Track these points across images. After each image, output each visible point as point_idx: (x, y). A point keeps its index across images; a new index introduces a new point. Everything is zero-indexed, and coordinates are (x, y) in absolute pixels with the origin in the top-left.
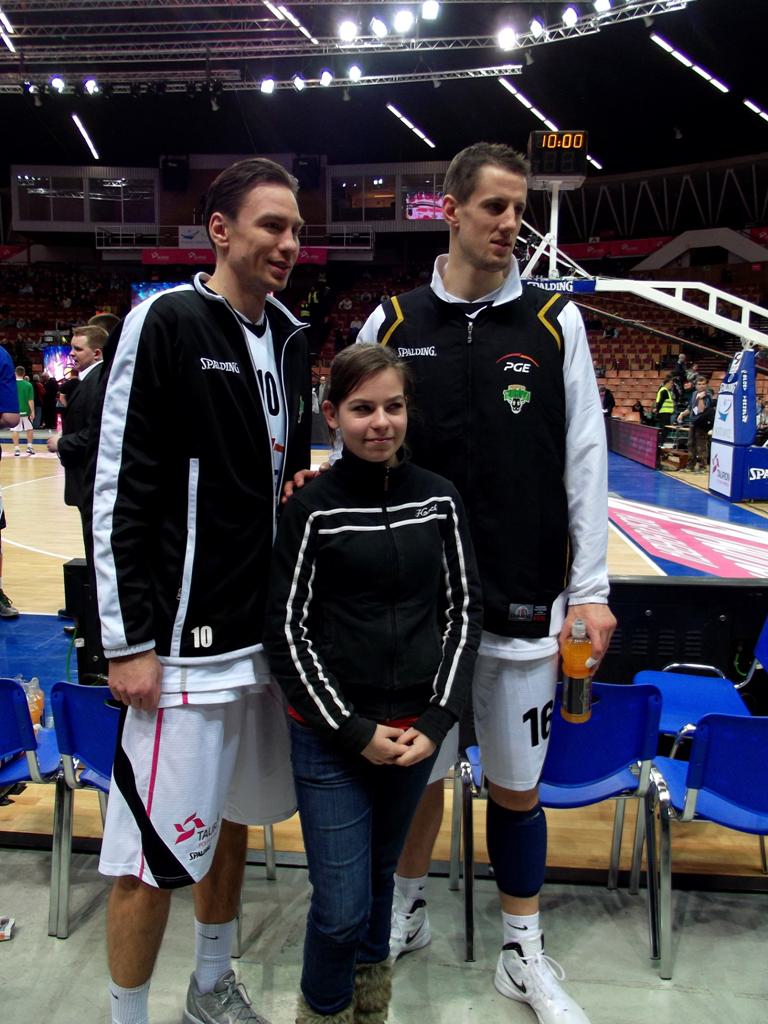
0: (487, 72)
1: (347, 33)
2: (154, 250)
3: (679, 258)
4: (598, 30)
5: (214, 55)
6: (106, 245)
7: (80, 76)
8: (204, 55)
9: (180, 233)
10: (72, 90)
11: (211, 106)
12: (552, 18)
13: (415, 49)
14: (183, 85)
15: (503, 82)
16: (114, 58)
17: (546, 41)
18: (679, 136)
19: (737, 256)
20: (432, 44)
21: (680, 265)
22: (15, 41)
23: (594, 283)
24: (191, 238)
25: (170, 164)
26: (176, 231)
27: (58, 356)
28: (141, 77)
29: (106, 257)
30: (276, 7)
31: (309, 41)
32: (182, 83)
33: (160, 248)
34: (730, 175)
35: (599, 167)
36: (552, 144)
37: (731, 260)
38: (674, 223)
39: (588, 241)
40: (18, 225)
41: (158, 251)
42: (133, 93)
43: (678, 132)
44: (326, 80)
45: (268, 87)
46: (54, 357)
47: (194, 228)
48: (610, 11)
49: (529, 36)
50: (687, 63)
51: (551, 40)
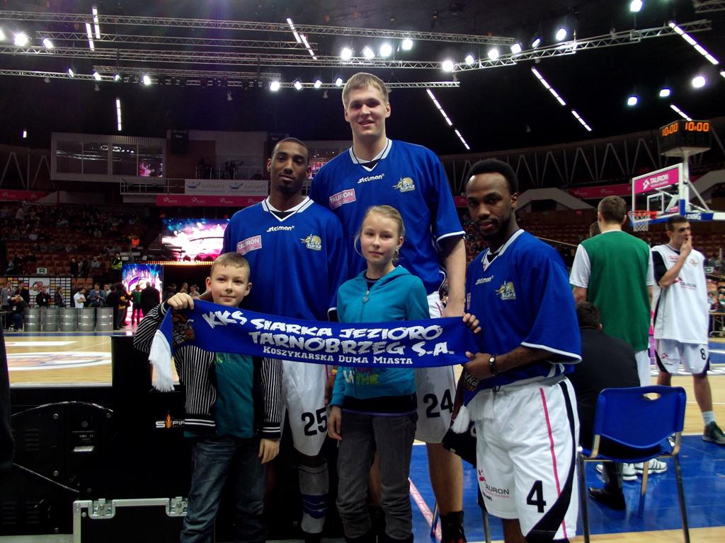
0: (419, 85)
1: (346, 55)
2: (166, 196)
3: (525, 206)
4: (515, 64)
5: (262, 63)
6: (126, 192)
7: (266, 75)
8: (255, 63)
9: (186, 184)
10: (157, 82)
11: (227, 97)
12: (480, 52)
13: (402, 67)
14: (199, 81)
15: (429, 92)
16: (234, 62)
17: (480, 68)
18: (529, 130)
19: (563, 205)
20: (413, 65)
21: (525, 211)
22: (97, 44)
23: (712, 215)
24: (194, 187)
25: (177, 136)
26: (183, 183)
27: (134, 271)
28: (209, 74)
29: (126, 200)
30: (299, 34)
31: (311, 58)
32: (239, 80)
33: (171, 194)
34: (550, 155)
35: (468, 148)
36: (691, 128)
37: (559, 208)
38: (542, 181)
39: (460, 195)
40: (55, 175)
41: (169, 196)
42: (244, 87)
43: (528, 128)
44: (318, 85)
45: (275, 86)
46: (130, 272)
47: (196, 181)
48: (521, 53)
49: (464, 64)
50: (547, 86)
51: (483, 67)
